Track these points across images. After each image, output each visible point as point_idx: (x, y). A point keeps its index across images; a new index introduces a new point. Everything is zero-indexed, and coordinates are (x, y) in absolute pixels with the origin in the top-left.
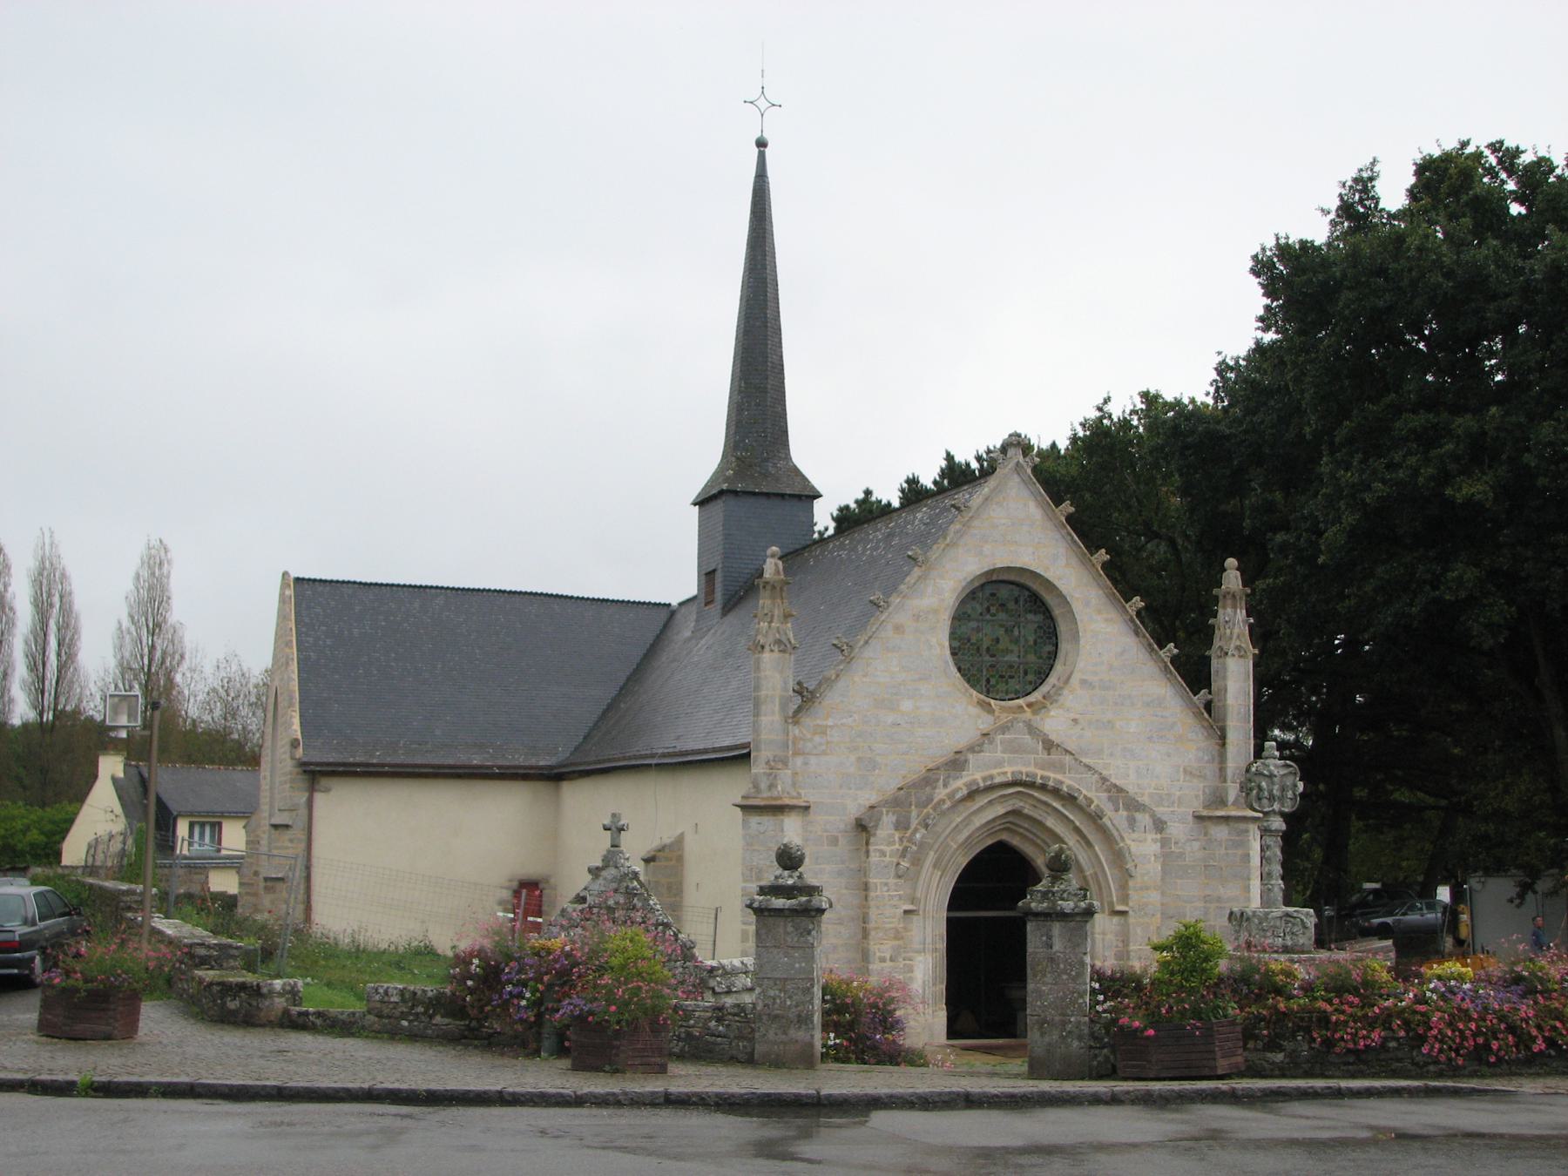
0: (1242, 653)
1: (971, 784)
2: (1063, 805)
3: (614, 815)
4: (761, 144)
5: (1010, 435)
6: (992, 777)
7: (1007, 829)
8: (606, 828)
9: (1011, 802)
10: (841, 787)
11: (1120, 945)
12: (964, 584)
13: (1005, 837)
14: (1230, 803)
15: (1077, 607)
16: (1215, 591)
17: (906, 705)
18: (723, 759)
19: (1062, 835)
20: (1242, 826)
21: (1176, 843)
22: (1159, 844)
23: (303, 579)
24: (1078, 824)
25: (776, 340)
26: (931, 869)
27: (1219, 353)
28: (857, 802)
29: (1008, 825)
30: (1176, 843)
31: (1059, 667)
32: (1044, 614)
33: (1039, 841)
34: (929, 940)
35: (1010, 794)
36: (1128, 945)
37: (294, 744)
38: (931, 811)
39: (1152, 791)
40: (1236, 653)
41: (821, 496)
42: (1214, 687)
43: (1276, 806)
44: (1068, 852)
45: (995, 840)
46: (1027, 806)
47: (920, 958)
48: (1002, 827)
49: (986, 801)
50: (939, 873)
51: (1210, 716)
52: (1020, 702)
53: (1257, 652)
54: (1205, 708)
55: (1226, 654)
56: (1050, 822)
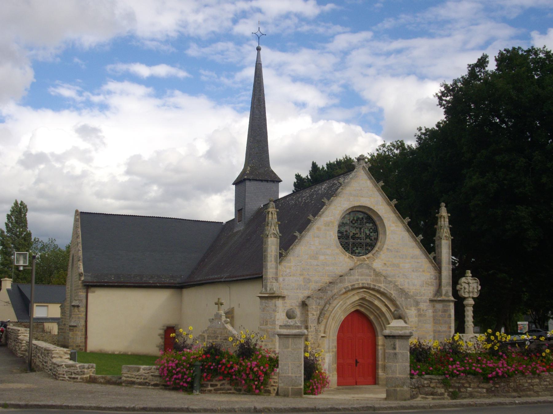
2: (381, 296)
3: (219, 299)
5: (360, 156)
6: (354, 285)
7: (359, 305)
8: (216, 304)
10: (297, 289)
12: (343, 212)
13: (358, 308)
14: (443, 295)
15: (385, 222)
17: (322, 257)
18: (237, 280)
20: (448, 304)
22: (417, 311)
23: (83, 212)
24: (387, 303)
25: (265, 123)
26: (331, 320)
27: (415, 136)
28: (302, 295)
31: (379, 244)
32: (373, 224)
33: (372, 310)
35: (361, 292)
37: (80, 275)
39: (414, 290)
40: (445, 238)
41: (282, 181)
42: (436, 251)
43: (471, 295)
45: (355, 309)
46: (367, 296)
47: (327, 355)
48: (358, 304)
52: (364, 257)
53: (452, 238)
55: (441, 238)
56: (376, 302)
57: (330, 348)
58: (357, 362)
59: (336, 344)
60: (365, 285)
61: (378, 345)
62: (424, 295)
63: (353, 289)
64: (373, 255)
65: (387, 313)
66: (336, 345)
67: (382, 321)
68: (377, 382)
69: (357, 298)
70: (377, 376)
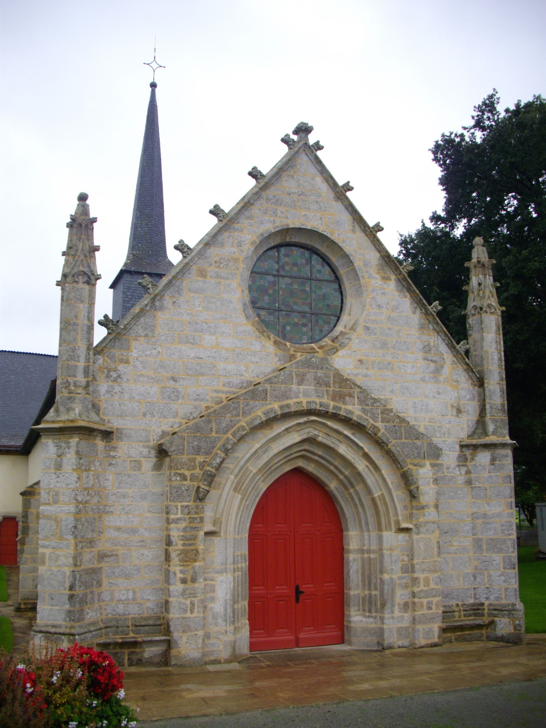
0: (493, 310)
1: (268, 412)
2: (353, 434)
4: (153, 86)
6: (288, 406)
7: (303, 457)
9: (306, 430)
11: (406, 559)
13: (300, 463)
14: (490, 433)
16: (466, 264)
19: (353, 461)
21: (448, 468)
24: (366, 450)
29: (304, 453)
30: (448, 468)
33: (332, 468)
34: (230, 560)
36: (412, 559)
38: (231, 437)
39: (426, 423)
44: (130, 616)
46: (321, 434)
47: (220, 578)
49: (283, 428)
50: (240, 496)
51: (468, 359)
53: (504, 309)
54: (465, 355)
56: (343, 449)
57: (228, 562)
58: (298, 592)
59: (245, 550)
60: (313, 407)
61: (349, 551)
62: (449, 433)
63: (286, 416)
64: (333, 341)
65: (370, 474)
66: (247, 553)
67: (357, 493)
68: (346, 637)
69: (295, 438)
70: (345, 623)
